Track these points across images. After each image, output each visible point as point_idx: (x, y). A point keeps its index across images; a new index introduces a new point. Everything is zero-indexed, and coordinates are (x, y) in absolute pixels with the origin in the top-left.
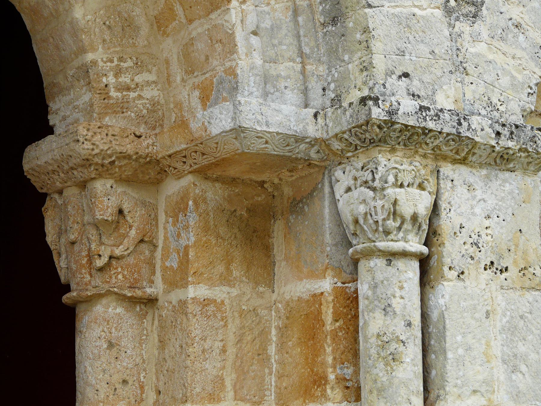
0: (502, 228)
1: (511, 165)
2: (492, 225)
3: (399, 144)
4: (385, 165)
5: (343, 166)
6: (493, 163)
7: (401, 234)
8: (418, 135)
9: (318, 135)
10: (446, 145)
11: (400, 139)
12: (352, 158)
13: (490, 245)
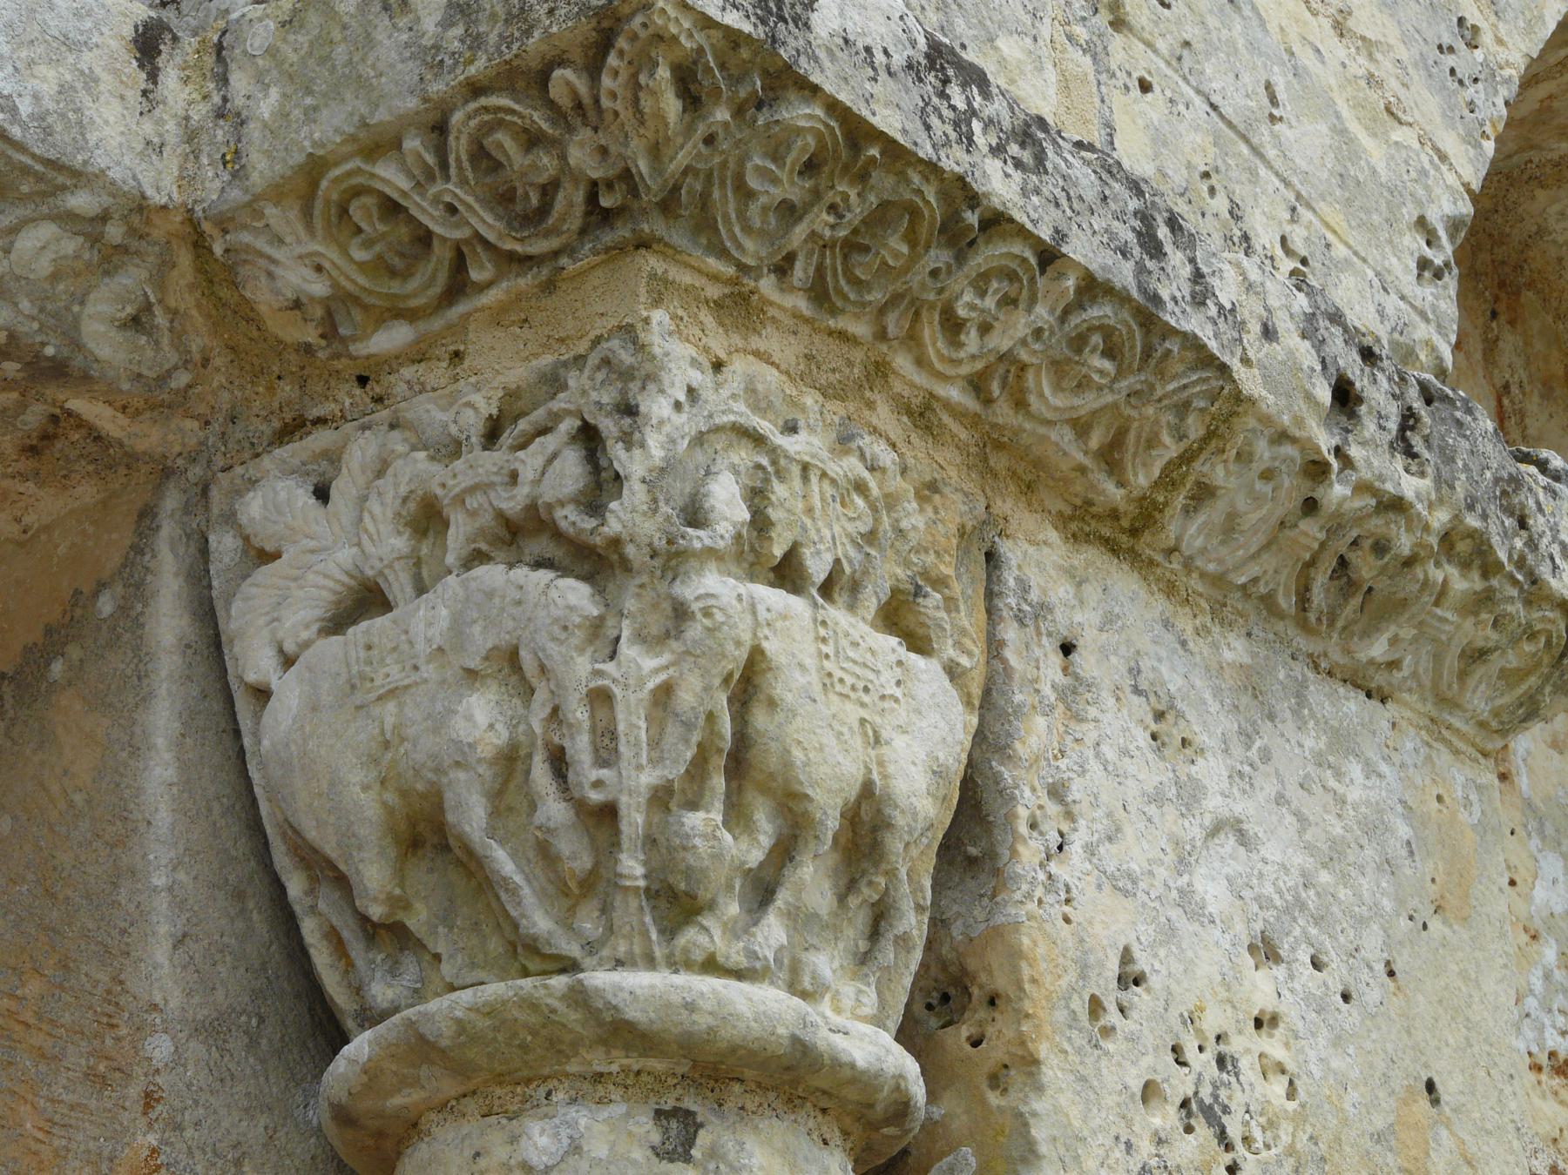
0: (1337, 1041)
1: (1378, 649)
2: (1290, 1009)
3: (783, 269)
4: (691, 391)
5: (321, 439)
6: (1287, 602)
7: (772, 932)
8: (911, 238)
9: (160, 182)
10: (1059, 368)
11: (800, 232)
12: (408, 372)
13: (1285, 1139)
